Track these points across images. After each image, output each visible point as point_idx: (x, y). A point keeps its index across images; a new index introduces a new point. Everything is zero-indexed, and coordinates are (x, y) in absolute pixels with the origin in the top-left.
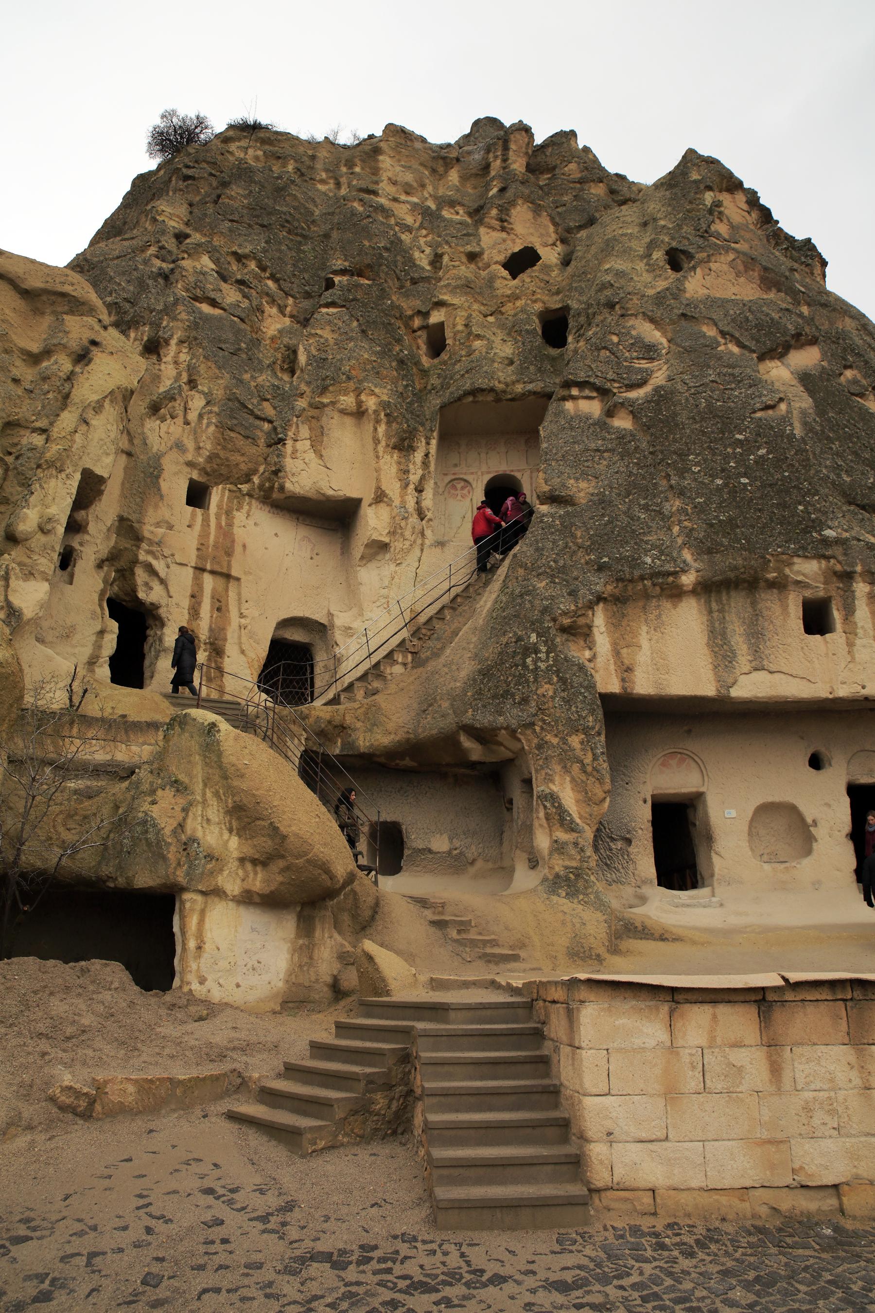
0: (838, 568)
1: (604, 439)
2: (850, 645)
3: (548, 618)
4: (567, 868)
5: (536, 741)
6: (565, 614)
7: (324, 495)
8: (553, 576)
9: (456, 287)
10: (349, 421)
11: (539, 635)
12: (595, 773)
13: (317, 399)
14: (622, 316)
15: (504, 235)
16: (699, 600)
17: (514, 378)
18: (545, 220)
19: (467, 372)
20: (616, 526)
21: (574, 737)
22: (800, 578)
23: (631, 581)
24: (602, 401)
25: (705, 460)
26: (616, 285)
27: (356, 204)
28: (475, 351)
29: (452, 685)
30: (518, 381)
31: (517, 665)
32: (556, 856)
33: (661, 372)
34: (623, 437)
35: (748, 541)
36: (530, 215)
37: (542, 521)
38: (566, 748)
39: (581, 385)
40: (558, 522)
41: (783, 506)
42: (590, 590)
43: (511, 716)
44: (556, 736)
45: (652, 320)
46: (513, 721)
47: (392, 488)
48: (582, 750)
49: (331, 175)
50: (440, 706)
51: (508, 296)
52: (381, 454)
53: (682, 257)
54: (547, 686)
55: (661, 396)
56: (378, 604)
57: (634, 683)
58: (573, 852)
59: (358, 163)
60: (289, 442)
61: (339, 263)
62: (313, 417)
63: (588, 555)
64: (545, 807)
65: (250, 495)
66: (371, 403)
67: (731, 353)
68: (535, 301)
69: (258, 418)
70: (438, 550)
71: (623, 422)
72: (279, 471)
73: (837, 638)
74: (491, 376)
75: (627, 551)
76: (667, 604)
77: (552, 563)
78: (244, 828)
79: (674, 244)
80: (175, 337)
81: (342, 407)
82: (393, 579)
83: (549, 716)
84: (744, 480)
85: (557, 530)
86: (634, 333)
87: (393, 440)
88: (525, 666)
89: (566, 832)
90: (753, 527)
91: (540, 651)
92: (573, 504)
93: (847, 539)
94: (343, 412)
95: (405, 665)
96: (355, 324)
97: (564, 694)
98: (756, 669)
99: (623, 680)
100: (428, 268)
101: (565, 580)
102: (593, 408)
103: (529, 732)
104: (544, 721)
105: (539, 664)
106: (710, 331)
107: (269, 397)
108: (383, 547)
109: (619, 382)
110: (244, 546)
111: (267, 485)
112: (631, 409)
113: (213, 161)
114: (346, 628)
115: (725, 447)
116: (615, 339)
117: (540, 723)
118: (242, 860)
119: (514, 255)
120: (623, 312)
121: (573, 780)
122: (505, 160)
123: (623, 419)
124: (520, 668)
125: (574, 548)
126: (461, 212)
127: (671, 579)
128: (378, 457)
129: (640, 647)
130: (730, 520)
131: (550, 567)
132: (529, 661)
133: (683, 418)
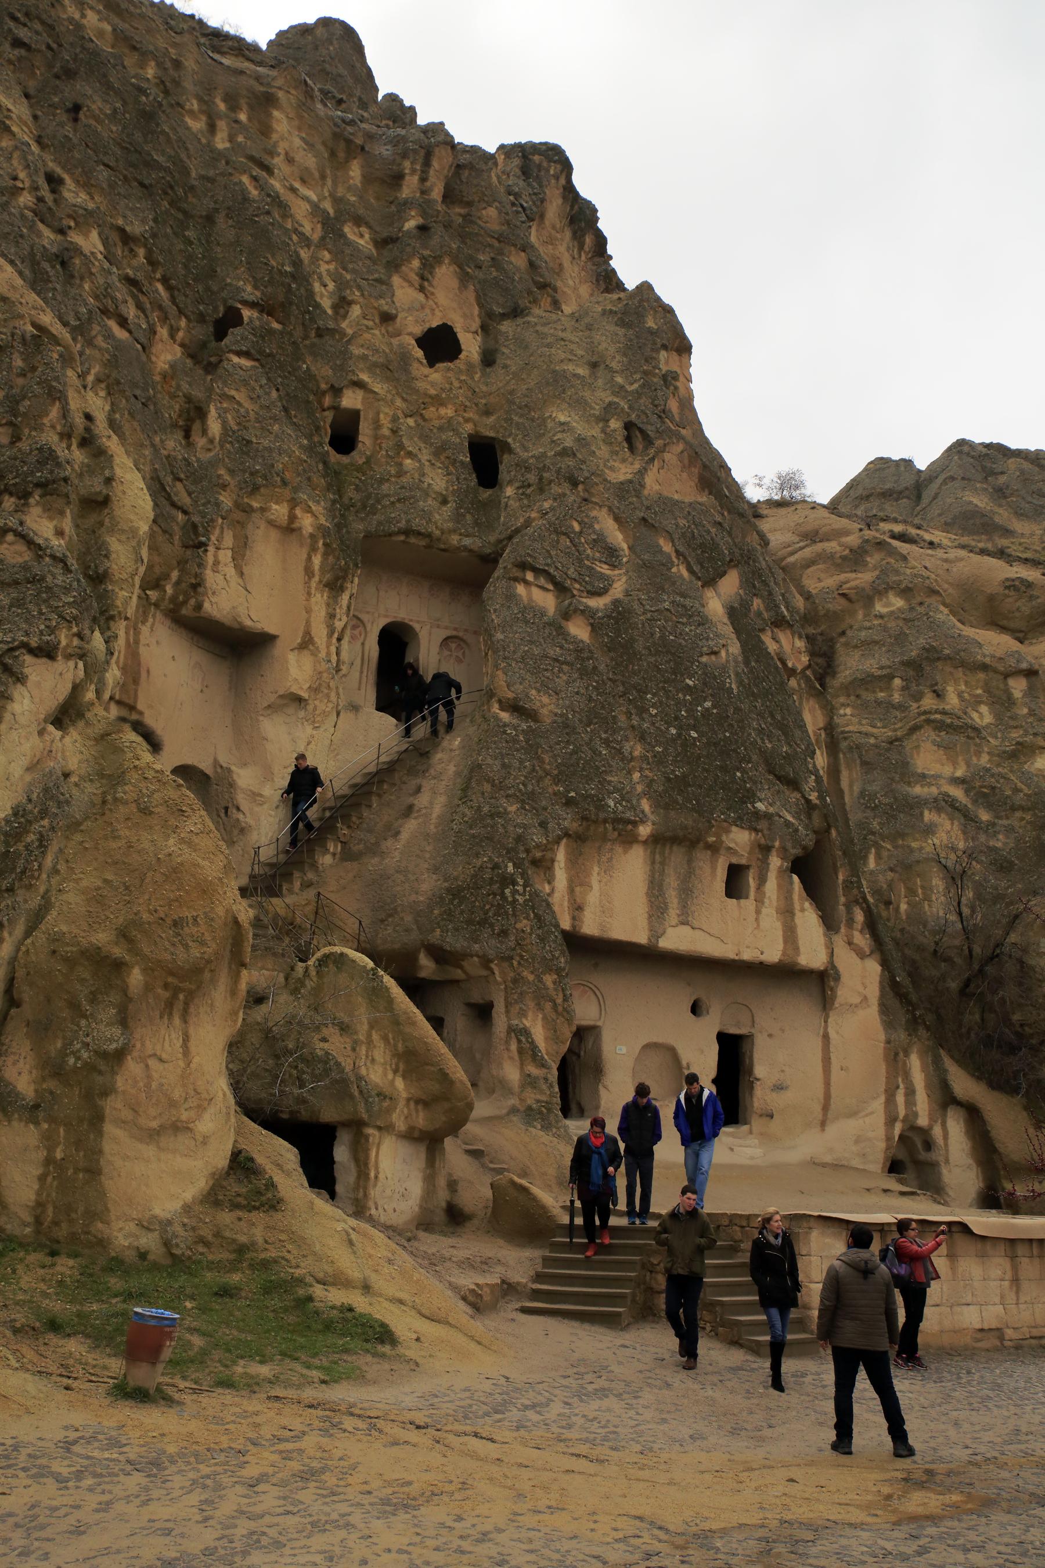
0: (763, 841)
1: (561, 647)
2: (758, 912)
3: (522, 848)
4: (538, 1101)
5: (512, 974)
6: (538, 846)
7: (240, 623)
8: (523, 802)
9: (375, 365)
10: (274, 534)
14: (585, 500)
15: (421, 297)
16: (645, 850)
17: (450, 525)
18: (470, 294)
19: (399, 500)
22: (732, 845)
24: (557, 598)
25: (661, 702)
26: (579, 456)
27: (245, 179)
29: (413, 897)
30: (455, 531)
31: (495, 895)
32: (529, 1090)
34: (581, 651)
35: (698, 801)
36: (455, 283)
37: (505, 732)
39: (536, 571)
41: (724, 769)
42: (559, 824)
43: (489, 945)
45: (617, 519)
47: (320, 633)
48: (556, 990)
49: (204, 108)
50: (402, 919)
51: (430, 397)
52: (313, 591)
53: (637, 433)
55: (619, 613)
58: (544, 1087)
59: (245, 107)
60: (211, 549)
61: (250, 292)
64: (519, 1041)
65: (156, 605)
66: (307, 523)
67: (681, 576)
68: (467, 420)
69: (174, 505)
70: (351, 715)
71: (579, 630)
72: (199, 585)
73: (748, 904)
74: (427, 515)
75: (592, 789)
76: (619, 849)
79: (633, 417)
80: (93, 372)
82: (309, 743)
84: (694, 734)
85: (522, 748)
86: (597, 527)
87: (328, 576)
88: (503, 894)
89: (537, 1067)
90: (700, 787)
91: (517, 884)
93: (772, 815)
94: (271, 523)
95: (334, 855)
96: (274, 394)
97: (540, 932)
98: (683, 924)
99: (574, 918)
100: (330, 312)
102: (546, 601)
103: (506, 964)
104: (522, 957)
106: (667, 547)
107: (182, 476)
108: (299, 700)
110: (148, 672)
111: (181, 598)
113: (50, 21)
114: (254, 793)
115: (678, 692)
116: (577, 527)
118: (408, 1100)
119: (431, 331)
120: (586, 495)
121: (545, 1018)
122: (423, 180)
125: (540, 773)
126: (367, 236)
127: (630, 827)
128: (309, 594)
130: (684, 776)
131: (520, 791)
132: (507, 891)
133: (639, 646)
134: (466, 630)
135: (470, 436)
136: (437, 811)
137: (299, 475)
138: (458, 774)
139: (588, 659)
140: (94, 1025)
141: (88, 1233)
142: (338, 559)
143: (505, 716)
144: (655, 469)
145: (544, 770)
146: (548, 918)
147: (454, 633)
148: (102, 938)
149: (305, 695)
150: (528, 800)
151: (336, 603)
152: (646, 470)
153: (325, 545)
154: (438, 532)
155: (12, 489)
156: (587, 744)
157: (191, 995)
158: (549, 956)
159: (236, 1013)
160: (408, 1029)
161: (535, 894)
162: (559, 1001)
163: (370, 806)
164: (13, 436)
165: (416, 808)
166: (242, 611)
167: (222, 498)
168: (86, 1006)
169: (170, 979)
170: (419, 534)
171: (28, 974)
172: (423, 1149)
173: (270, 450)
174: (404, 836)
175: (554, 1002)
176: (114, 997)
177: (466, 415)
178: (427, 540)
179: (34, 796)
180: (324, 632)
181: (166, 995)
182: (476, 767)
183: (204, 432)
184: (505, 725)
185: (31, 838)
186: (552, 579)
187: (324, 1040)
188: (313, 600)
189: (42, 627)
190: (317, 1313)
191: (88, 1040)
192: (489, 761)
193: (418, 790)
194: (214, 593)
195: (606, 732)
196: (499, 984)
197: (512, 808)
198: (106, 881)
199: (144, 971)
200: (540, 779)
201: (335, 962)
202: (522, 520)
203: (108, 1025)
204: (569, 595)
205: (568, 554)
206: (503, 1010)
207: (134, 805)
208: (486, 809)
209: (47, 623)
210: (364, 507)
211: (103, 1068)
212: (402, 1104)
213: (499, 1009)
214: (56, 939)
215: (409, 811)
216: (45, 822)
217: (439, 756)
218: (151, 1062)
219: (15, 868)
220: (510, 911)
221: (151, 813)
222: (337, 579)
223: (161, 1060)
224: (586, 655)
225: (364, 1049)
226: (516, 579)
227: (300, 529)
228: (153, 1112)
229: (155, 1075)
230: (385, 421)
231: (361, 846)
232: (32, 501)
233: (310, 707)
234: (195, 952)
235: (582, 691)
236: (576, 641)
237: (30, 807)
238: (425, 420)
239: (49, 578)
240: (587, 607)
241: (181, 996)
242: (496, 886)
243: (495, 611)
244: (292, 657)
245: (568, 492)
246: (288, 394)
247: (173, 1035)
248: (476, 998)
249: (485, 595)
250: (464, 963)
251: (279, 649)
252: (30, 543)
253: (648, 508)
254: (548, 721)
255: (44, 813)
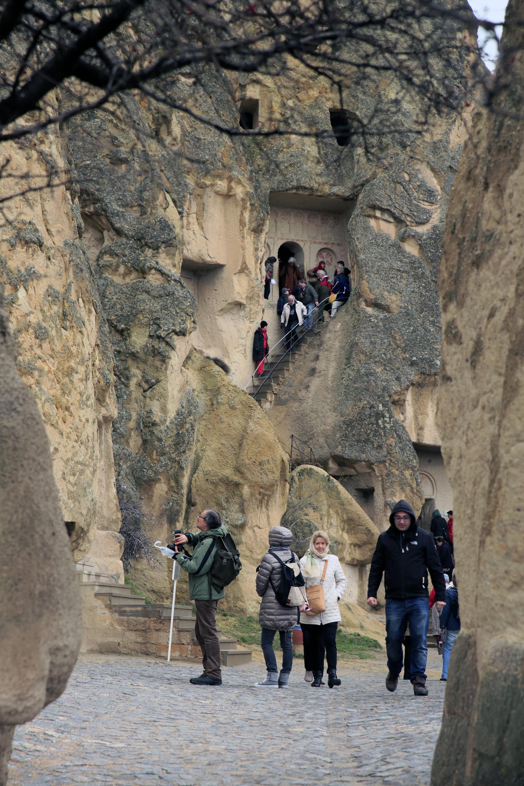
3: (386, 394)
5: (386, 471)
6: (396, 393)
7: (203, 260)
8: (385, 365)
10: (219, 199)
11: (383, 406)
12: (418, 493)
13: (202, 180)
14: (412, 158)
19: (290, 165)
20: (418, 335)
21: (406, 471)
23: (429, 375)
24: (396, 227)
28: (293, 145)
29: (323, 427)
31: (373, 424)
33: (436, 214)
34: (414, 263)
37: (370, 321)
38: (403, 477)
39: (383, 210)
40: (381, 324)
42: (407, 378)
43: (371, 455)
44: (398, 470)
45: (433, 170)
46: (372, 458)
48: (412, 479)
50: (318, 440)
52: (245, 235)
54: (392, 439)
55: (437, 235)
56: (238, 350)
57: (423, 437)
62: (198, 195)
63: (405, 353)
66: (239, 191)
68: (328, 100)
75: (426, 354)
77: (383, 355)
78: (351, 529)
81: (218, 189)
83: (394, 457)
86: (420, 176)
87: (254, 225)
88: (377, 424)
92: (389, 312)
94: (217, 193)
95: (271, 402)
97: (400, 445)
99: (418, 435)
101: (392, 369)
103: (381, 466)
104: (391, 460)
105: (386, 425)
108: (239, 305)
109: (411, 218)
112: (420, 242)
116: (407, 178)
117: (389, 462)
118: (351, 544)
120: (412, 154)
123: (411, 246)
124: (375, 426)
125: (394, 346)
129: (427, 415)
131: (383, 358)
134: (333, 244)
135: (330, 109)
136: (331, 372)
137: (231, 158)
138: (342, 348)
139: (418, 268)
140: (229, 513)
141: (236, 607)
142: (259, 213)
143: (370, 310)
144: (456, 128)
145: (396, 344)
146: (404, 436)
147: (325, 246)
148: (228, 472)
149: (244, 302)
150: (387, 363)
151: (258, 240)
152: (450, 130)
153: (252, 205)
154: (316, 186)
155: (150, 245)
156: (422, 325)
157: (269, 496)
158: (407, 459)
159: (284, 505)
160: (348, 507)
161: (396, 422)
162: (414, 486)
163: (289, 370)
164: (141, 212)
165: (318, 371)
166: (204, 252)
167: (188, 181)
168: (224, 504)
169: (261, 490)
170: (305, 188)
171: (197, 491)
172: (357, 570)
173: (211, 143)
174: (312, 388)
175: (411, 486)
176: (237, 499)
177: (327, 95)
178: (310, 191)
179: (184, 405)
180: (253, 260)
181: (260, 497)
182: (353, 345)
183: (169, 133)
184: (370, 316)
185: (188, 426)
186: (393, 215)
187: (306, 515)
188: (246, 241)
189: (180, 321)
190: (345, 636)
191: (228, 520)
192: (362, 340)
193: (317, 358)
194: (188, 243)
195: (432, 316)
196: (378, 477)
197: (379, 370)
198: (222, 444)
199: (250, 487)
200: (394, 350)
201: (307, 474)
202: (370, 173)
203: (235, 512)
204: (404, 225)
205: (403, 197)
206: (381, 492)
207: (227, 405)
208: (363, 371)
209: (181, 318)
210: (268, 171)
211: (236, 532)
212: (348, 546)
213: (378, 491)
214: (206, 474)
215: (313, 372)
216: (191, 417)
217: (328, 335)
218: (256, 529)
219: (184, 441)
220: (383, 434)
221: (236, 409)
222: (259, 226)
223: (259, 528)
224: (417, 265)
225: (326, 519)
226: (369, 216)
227: (235, 195)
228: (259, 551)
229: (258, 535)
230: (276, 107)
231: (287, 396)
232: (160, 250)
233: (247, 309)
234: (271, 477)
235: (416, 290)
236: (410, 256)
237: (183, 410)
238: (300, 101)
239: (176, 293)
240: (416, 233)
241: (266, 498)
242: (373, 419)
243: (358, 239)
244: (235, 279)
245: (400, 152)
246: (217, 99)
247: (263, 516)
248: (363, 485)
249: (349, 226)
250: (356, 466)
251: (225, 273)
252: (162, 274)
253: (453, 158)
254: (396, 312)
255: (190, 413)
